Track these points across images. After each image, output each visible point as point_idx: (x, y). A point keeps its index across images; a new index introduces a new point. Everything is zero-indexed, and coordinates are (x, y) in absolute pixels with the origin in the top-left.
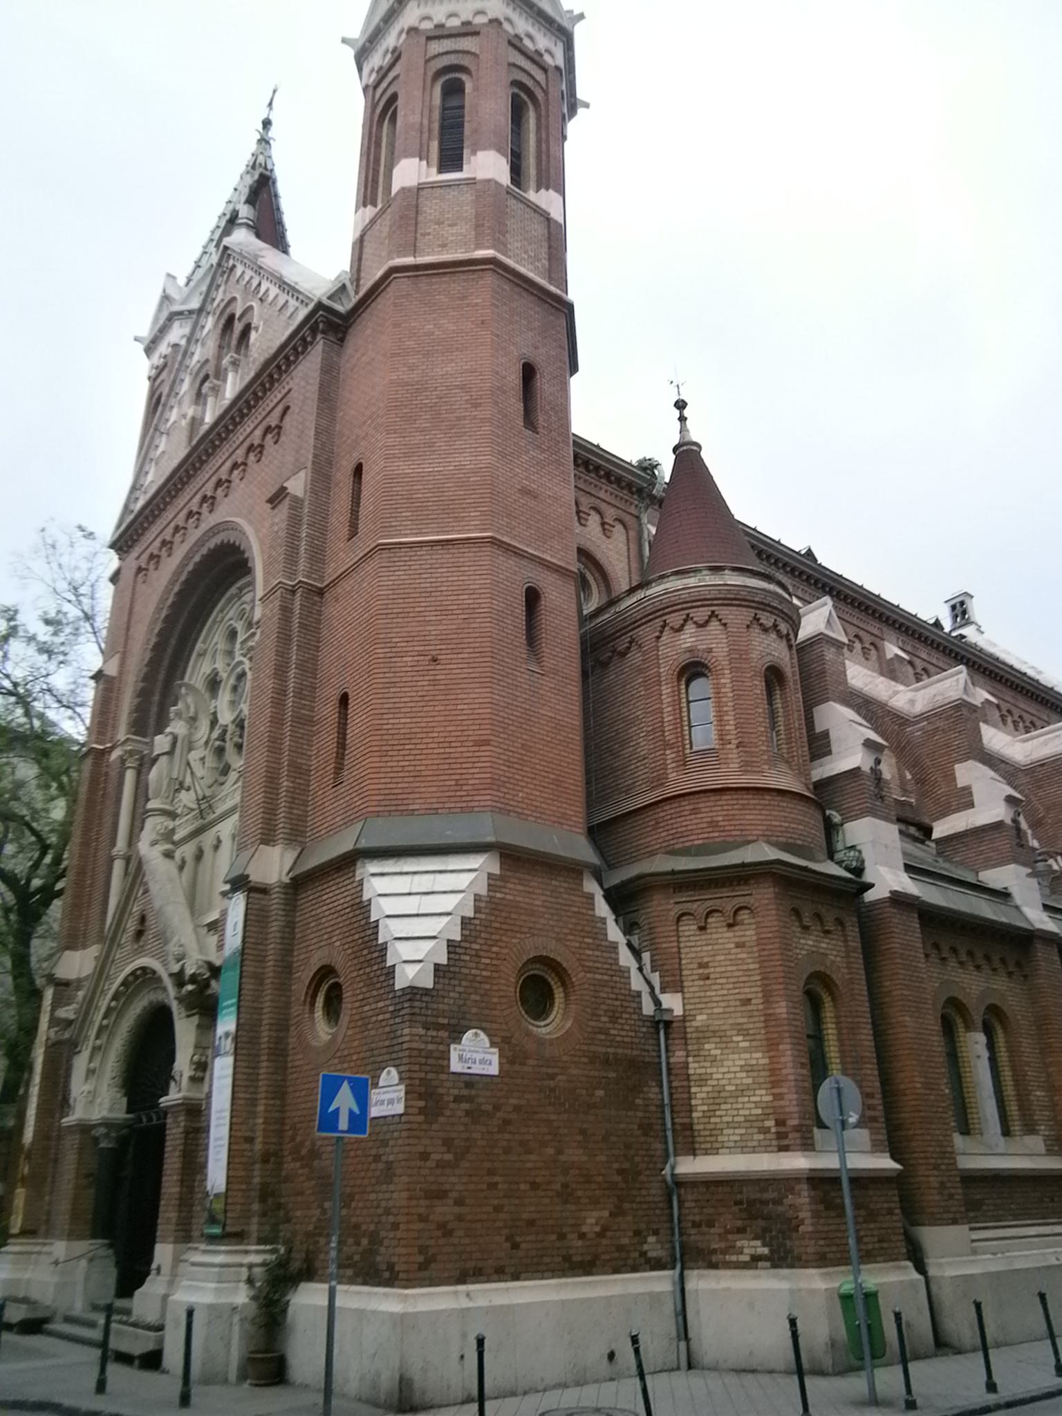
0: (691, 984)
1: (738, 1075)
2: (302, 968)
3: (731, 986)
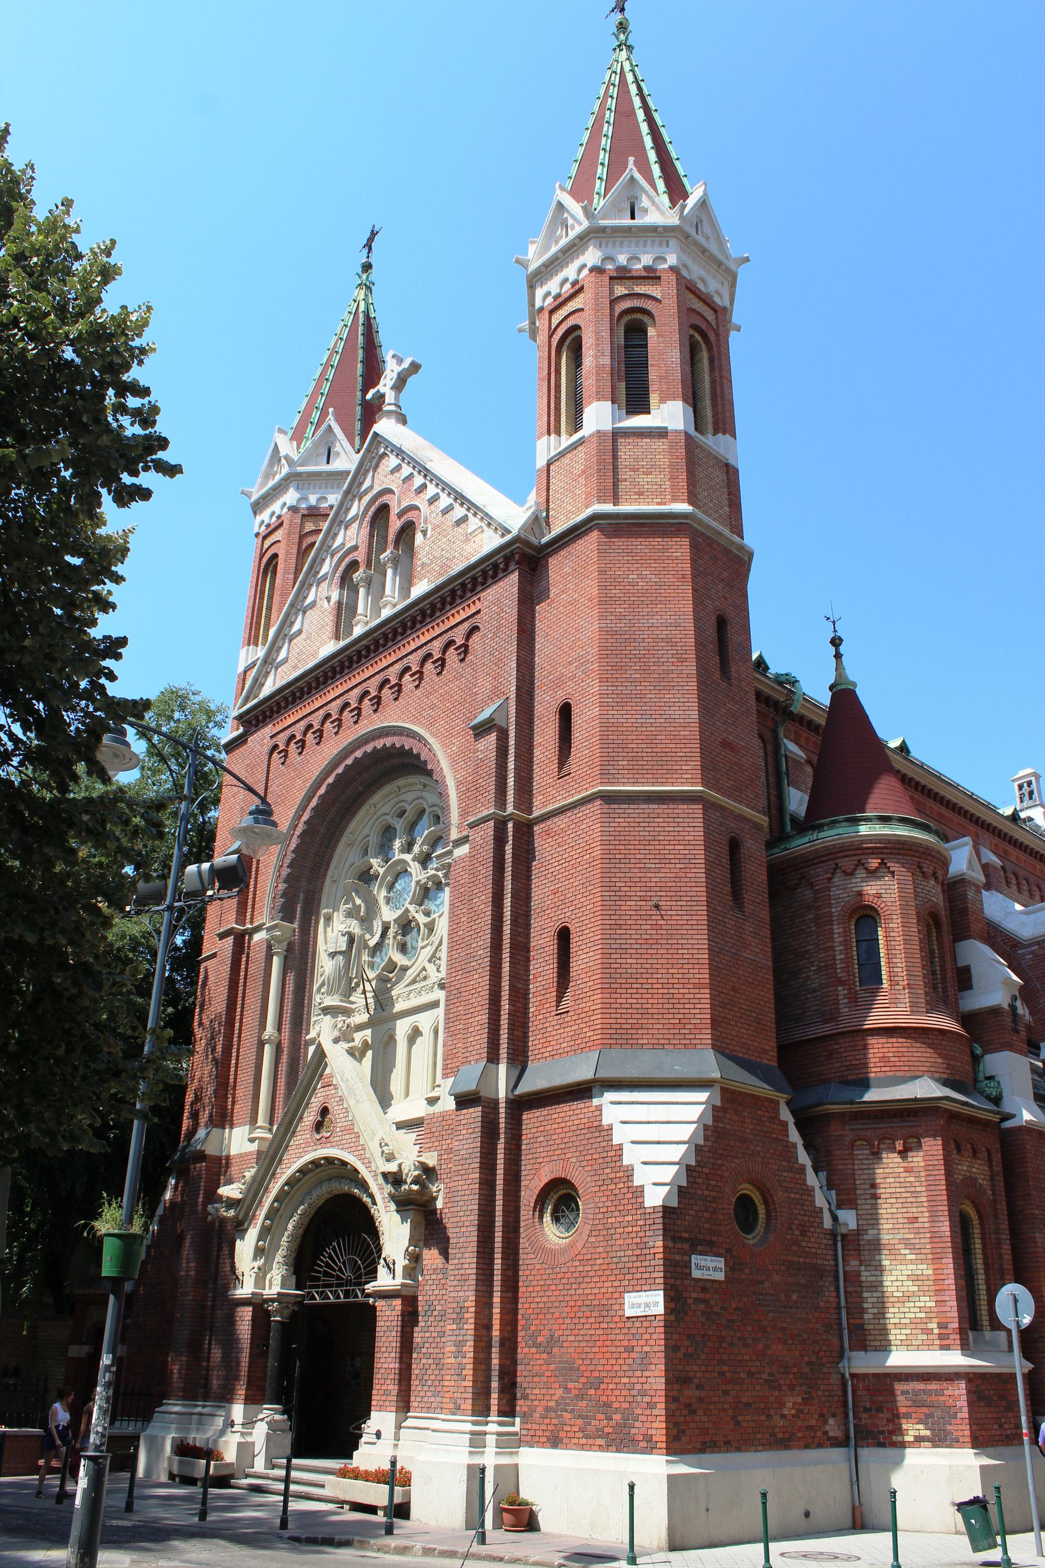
0: (863, 1202)
1: (905, 1283)
2: (530, 1177)
3: (900, 1205)
